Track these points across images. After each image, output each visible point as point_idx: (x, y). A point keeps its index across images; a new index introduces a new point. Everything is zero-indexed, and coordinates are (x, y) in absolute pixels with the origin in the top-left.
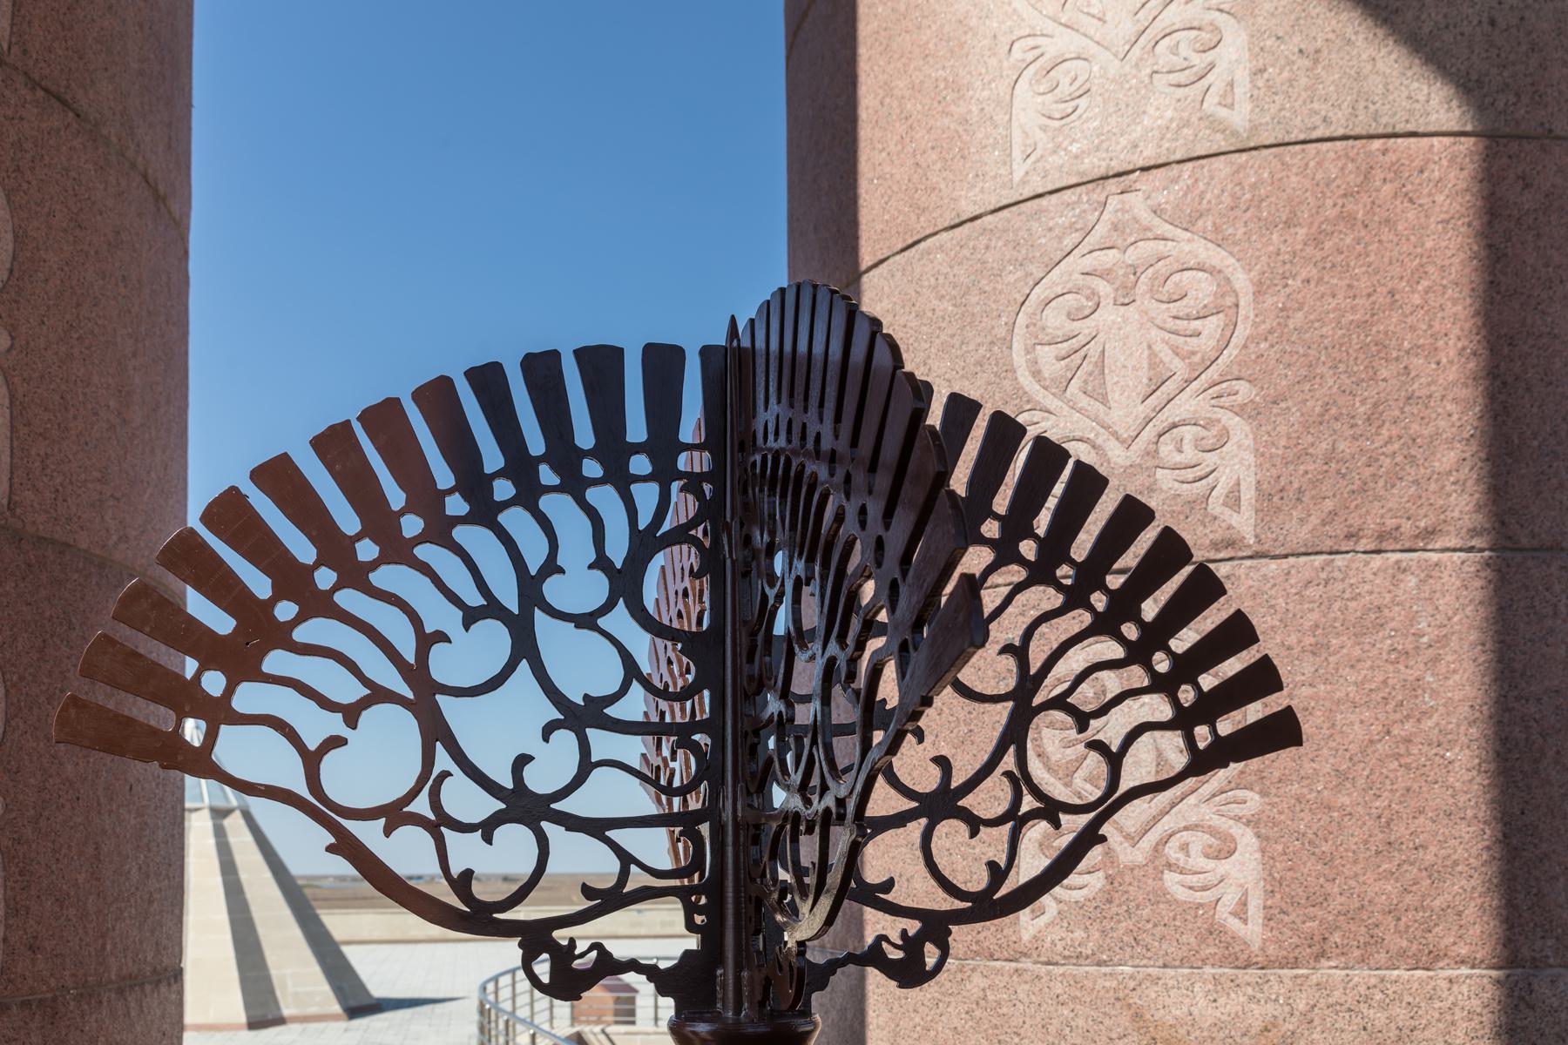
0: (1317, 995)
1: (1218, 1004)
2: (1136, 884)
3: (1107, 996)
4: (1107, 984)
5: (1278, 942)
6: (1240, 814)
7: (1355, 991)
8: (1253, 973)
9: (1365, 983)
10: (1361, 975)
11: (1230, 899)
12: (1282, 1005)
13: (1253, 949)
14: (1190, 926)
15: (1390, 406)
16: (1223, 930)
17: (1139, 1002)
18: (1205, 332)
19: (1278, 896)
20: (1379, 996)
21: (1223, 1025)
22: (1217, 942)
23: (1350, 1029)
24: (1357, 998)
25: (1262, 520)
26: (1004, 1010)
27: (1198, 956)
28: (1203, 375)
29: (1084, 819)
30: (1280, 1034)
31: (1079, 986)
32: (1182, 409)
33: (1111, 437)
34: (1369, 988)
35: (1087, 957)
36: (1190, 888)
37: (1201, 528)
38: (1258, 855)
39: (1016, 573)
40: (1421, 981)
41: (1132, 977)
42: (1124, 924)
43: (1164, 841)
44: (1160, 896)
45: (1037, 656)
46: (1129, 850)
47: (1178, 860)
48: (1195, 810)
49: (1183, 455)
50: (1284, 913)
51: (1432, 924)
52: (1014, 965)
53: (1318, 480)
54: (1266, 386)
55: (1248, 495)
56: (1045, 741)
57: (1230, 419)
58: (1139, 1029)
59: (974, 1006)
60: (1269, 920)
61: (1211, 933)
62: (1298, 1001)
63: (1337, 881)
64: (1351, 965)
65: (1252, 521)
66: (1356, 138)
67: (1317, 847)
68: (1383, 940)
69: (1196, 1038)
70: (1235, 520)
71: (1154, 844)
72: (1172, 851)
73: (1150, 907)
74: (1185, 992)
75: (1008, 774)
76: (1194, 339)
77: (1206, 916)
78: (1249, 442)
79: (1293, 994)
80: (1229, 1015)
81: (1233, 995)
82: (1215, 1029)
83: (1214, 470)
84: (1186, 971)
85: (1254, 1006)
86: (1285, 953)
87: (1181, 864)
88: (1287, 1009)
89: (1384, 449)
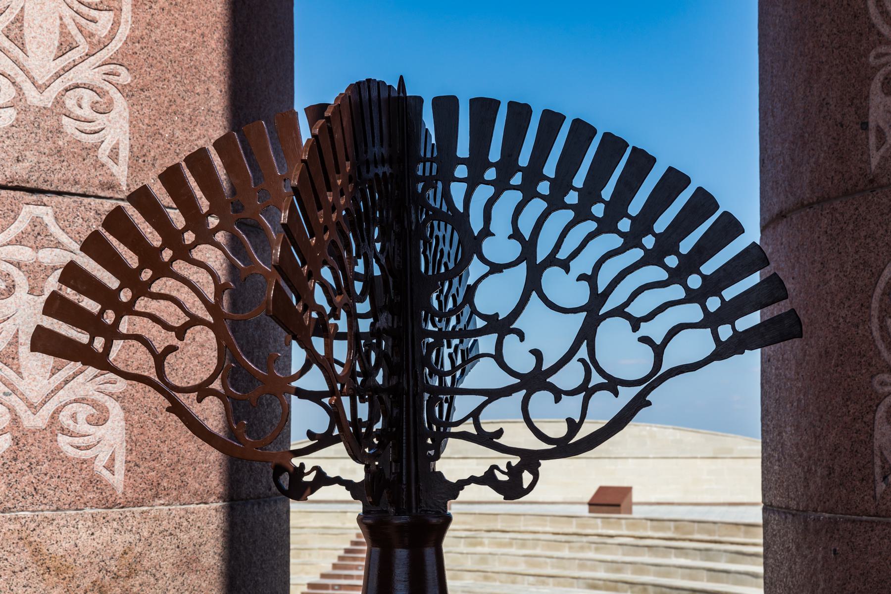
0: (154, 525)
1: (94, 537)
2: (37, 444)
3: (12, 537)
4: (12, 527)
5: (134, 488)
6: (113, 392)
7: (174, 521)
8: (115, 513)
9: (178, 515)
10: (177, 508)
11: (103, 458)
12: (134, 534)
13: (118, 493)
15: (200, 113)
16: (99, 480)
17: (38, 540)
18: (100, 23)
19: (134, 454)
20: (185, 524)
21: (98, 552)
22: (95, 488)
23: (171, 548)
24: (175, 525)
25: (132, 175)
27: (82, 501)
28: (98, 54)
30: (133, 555)
32: (83, 75)
33: (28, 80)
34: (180, 518)
36: (78, 447)
37: (93, 170)
38: (123, 423)
39: (591, 226)
40: (204, 511)
41: (33, 520)
42: (27, 477)
43: (58, 411)
44: (56, 455)
46: (32, 417)
47: (69, 425)
48: (83, 387)
49: (82, 111)
50: (137, 465)
51: (209, 472)
53: (164, 154)
54: (138, 76)
55: (124, 154)
57: (115, 93)
58: (37, 561)
60: (129, 471)
61: (91, 482)
62: (143, 530)
63: (166, 442)
64: (171, 502)
65: (126, 173)
67: (157, 418)
68: (188, 483)
69: (80, 564)
70: (115, 169)
71: (51, 412)
72: (64, 418)
73: (47, 463)
74: (72, 529)
75: (582, 360)
76: (93, 24)
77: (88, 469)
78: (126, 114)
79: (141, 525)
80: (102, 544)
81: (104, 529)
82: (93, 556)
83: (103, 129)
84: (73, 513)
85: (117, 536)
86: (137, 495)
87: (71, 428)
88: (137, 537)
89: (197, 142)
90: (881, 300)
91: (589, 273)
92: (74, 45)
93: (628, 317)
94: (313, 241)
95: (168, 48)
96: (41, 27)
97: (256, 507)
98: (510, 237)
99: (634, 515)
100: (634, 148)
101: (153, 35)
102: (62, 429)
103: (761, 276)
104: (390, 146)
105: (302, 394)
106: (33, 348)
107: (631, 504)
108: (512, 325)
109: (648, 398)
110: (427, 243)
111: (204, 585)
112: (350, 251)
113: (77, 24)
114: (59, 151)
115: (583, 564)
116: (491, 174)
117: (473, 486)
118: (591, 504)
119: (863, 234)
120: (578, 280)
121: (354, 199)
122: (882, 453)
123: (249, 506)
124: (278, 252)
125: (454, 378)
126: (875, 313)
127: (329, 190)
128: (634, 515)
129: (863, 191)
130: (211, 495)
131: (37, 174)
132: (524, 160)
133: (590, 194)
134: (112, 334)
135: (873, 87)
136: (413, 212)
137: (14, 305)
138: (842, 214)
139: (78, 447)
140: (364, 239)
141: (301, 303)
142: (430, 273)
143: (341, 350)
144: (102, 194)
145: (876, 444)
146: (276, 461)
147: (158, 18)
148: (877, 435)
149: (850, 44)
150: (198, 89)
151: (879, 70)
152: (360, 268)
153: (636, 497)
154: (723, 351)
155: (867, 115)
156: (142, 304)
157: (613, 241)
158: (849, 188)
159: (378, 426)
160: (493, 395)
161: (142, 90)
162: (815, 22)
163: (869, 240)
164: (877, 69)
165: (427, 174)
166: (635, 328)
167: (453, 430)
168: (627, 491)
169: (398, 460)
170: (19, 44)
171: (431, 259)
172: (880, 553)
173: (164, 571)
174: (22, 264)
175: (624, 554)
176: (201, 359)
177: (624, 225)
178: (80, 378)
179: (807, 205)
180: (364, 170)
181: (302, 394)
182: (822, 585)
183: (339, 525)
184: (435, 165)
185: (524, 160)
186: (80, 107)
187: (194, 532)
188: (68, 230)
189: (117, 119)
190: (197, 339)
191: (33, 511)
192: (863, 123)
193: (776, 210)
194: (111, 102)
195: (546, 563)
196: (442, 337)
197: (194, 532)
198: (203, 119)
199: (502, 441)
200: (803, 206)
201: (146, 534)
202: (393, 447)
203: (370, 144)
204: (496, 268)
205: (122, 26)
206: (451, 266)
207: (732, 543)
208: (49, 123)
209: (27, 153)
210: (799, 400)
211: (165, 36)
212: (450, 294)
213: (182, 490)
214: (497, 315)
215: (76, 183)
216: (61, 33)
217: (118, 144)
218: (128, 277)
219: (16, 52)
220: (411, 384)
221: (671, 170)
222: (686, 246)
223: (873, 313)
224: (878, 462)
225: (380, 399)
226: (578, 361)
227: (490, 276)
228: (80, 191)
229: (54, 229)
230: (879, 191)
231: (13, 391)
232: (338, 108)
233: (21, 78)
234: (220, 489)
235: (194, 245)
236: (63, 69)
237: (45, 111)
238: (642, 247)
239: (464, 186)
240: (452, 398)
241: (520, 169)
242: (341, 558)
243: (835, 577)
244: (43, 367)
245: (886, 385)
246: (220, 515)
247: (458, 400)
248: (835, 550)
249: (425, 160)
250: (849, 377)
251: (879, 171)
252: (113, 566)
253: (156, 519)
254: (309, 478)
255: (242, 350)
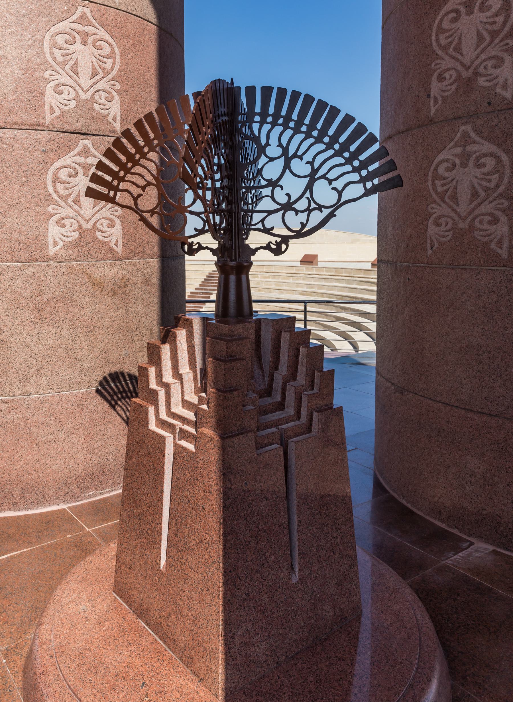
4: (80, 267)
5: (126, 252)
11: (114, 241)
14: (104, 248)
18: (108, 63)
26: (43, 279)
29: (330, 210)
31: (71, 269)
35: (73, 259)
38: (121, 227)
39: (312, 140)
41: (88, 265)
43: (96, 222)
44: (96, 240)
45: (317, 164)
46: (86, 225)
52: (46, 263)
55: (118, 118)
56: (57, 187)
59: (30, 279)
66: (142, 18)
70: (115, 124)
72: (98, 225)
75: (307, 198)
78: (119, 102)
87: (101, 229)
88: (127, 271)
90: (433, 172)
91: (311, 161)
92: (98, 73)
93: (327, 179)
94: (198, 147)
95: (135, 74)
96: (84, 66)
97: (172, 260)
98: (277, 146)
99: (318, 266)
100: (331, 106)
101: (128, 68)
102: (98, 230)
103: (379, 164)
104: (228, 108)
105: (192, 213)
106: (86, 196)
107: (317, 261)
108: (278, 183)
109: (335, 213)
110: (242, 149)
111: (153, 290)
112: (212, 152)
113: (98, 64)
114: (93, 118)
115: (298, 285)
116: (270, 119)
117: (262, 250)
118: (301, 262)
119: (426, 144)
120: (306, 164)
121: (214, 131)
122: (431, 238)
123: (170, 260)
124: (183, 152)
125: (253, 206)
126: (430, 178)
127: (204, 126)
128: (318, 266)
129: (427, 125)
130: (155, 256)
131: (85, 127)
132: (284, 113)
133: (312, 126)
134: (116, 189)
135: (433, 79)
136: (237, 136)
137: (78, 181)
138: (417, 136)
139: (104, 237)
140: (217, 147)
141: (193, 174)
142: (244, 162)
143: (209, 195)
144: (110, 135)
145: (428, 234)
146: (183, 240)
147: (130, 61)
148: (429, 230)
149: (423, 60)
150: (147, 91)
151: (436, 71)
152: (216, 161)
153: (319, 259)
154: (368, 193)
155: (430, 92)
156: (129, 177)
157: (321, 147)
158: (421, 124)
159: (223, 225)
160: (270, 213)
161: (125, 91)
162: (408, 51)
163: (429, 147)
164: (435, 70)
165: (242, 120)
166: (330, 184)
167: (253, 227)
168: (316, 256)
169: (231, 240)
170: (76, 74)
171: (244, 157)
172: (428, 280)
173: (138, 285)
174: (80, 164)
175: (314, 282)
176: (150, 201)
177: (326, 140)
178: (104, 209)
179: (401, 132)
180: (217, 118)
181: (192, 213)
182: (402, 292)
183: (202, 269)
184: (245, 116)
185: (284, 113)
186: (101, 99)
187: (149, 270)
188: (98, 150)
189: (115, 104)
190: (149, 194)
191: (88, 261)
192: (428, 95)
193: (387, 135)
194: (113, 97)
195: (283, 285)
196: (249, 189)
197: (149, 270)
198: (149, 103)
199: (273, 232)
200: (399, 133)
201: (130, 270)
202: (229, 234)
203: (220, 107)
204: (271, 159)
205: (116, 65)
206: (252, 160)
207: (358, 277)
208: (89, 106)
209: (81, 119)
210: (395, 216)
211: (133, 68)
212: (251, 172)
213: (144, 254)
214: (272, 179)
215: (100, 130)
216: (92, 68)
217: (116, 114)
218: (122, 166)
219: (75, 76)
220: (236, 208)
221: (347, 115)
222: (353, 148)
223: (429, 178)
224: (429, 241)
225: (224, 214)
226: (306, 198)
227: (269, 163)
228: (102, 134)
229: (92, 150)
230: (434, 125)
231: (79, 214)
232: (206, 91)
233: (78, 88)
234: (158, 253)
235: (148, 152)
236: (94, 83)
237: (87, 101)
238: (334, 149)
239: (258, 125)
240: (252, 215)
241: (282, 117)
242: (203, 282)
243: (408, 289)
244: (90, 205)
245: (434, 209)
246: (159, 263)
247: (255, 215)
248: (409, 278)
249: (241, 114)
250: (418, 206)
251: (434, 116)
252: (118, 283)
253: (134, 265)
254: (195, 247)
255: (168, 195)
